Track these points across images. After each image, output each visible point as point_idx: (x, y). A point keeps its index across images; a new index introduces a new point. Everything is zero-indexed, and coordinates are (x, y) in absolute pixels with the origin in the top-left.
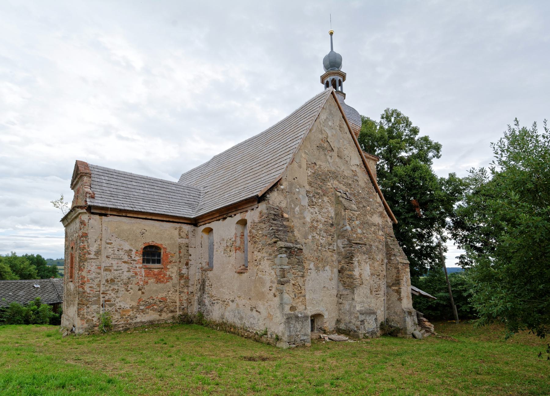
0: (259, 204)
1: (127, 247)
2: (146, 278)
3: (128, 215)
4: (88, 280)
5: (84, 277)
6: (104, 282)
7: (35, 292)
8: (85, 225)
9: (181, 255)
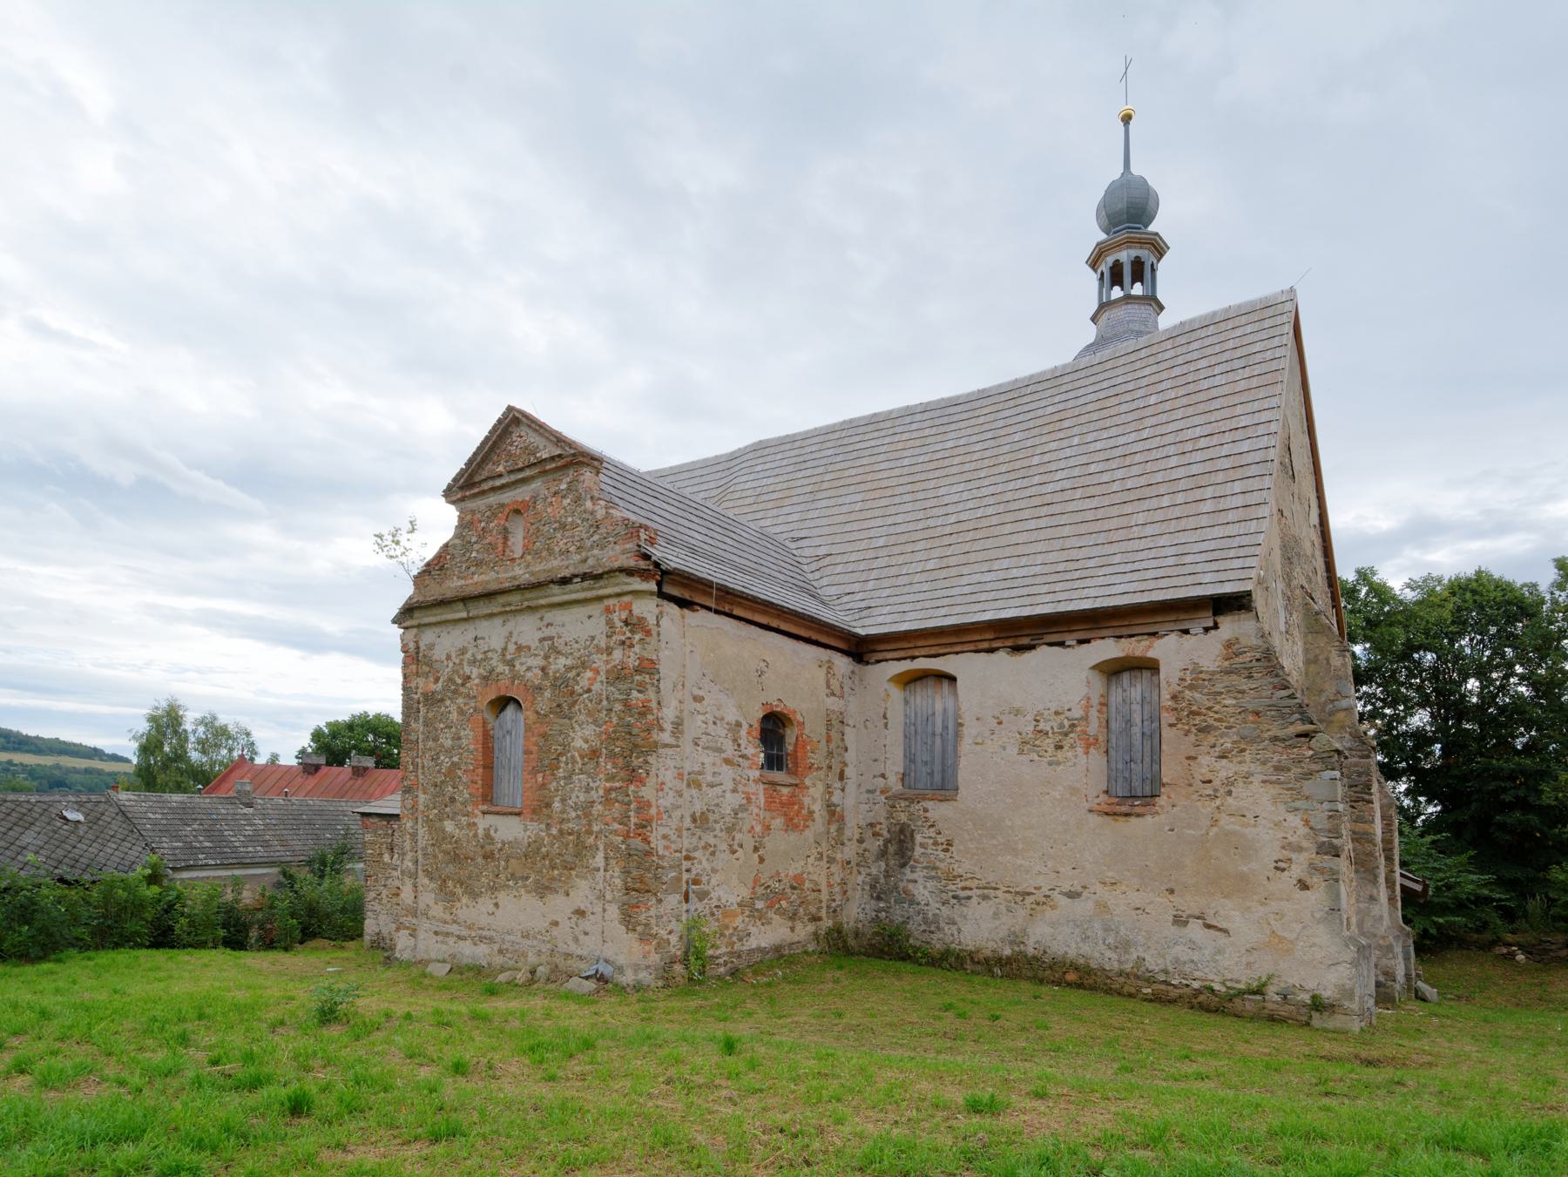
0: (1220, 619)
1: (732, 715)
2: (768, 814)
3: (737, 612)
4: (659, 813)
5: (649, 804)
6: (688, 822)
7: (73, 837)
8: (648, 633)
9: (832, 746)
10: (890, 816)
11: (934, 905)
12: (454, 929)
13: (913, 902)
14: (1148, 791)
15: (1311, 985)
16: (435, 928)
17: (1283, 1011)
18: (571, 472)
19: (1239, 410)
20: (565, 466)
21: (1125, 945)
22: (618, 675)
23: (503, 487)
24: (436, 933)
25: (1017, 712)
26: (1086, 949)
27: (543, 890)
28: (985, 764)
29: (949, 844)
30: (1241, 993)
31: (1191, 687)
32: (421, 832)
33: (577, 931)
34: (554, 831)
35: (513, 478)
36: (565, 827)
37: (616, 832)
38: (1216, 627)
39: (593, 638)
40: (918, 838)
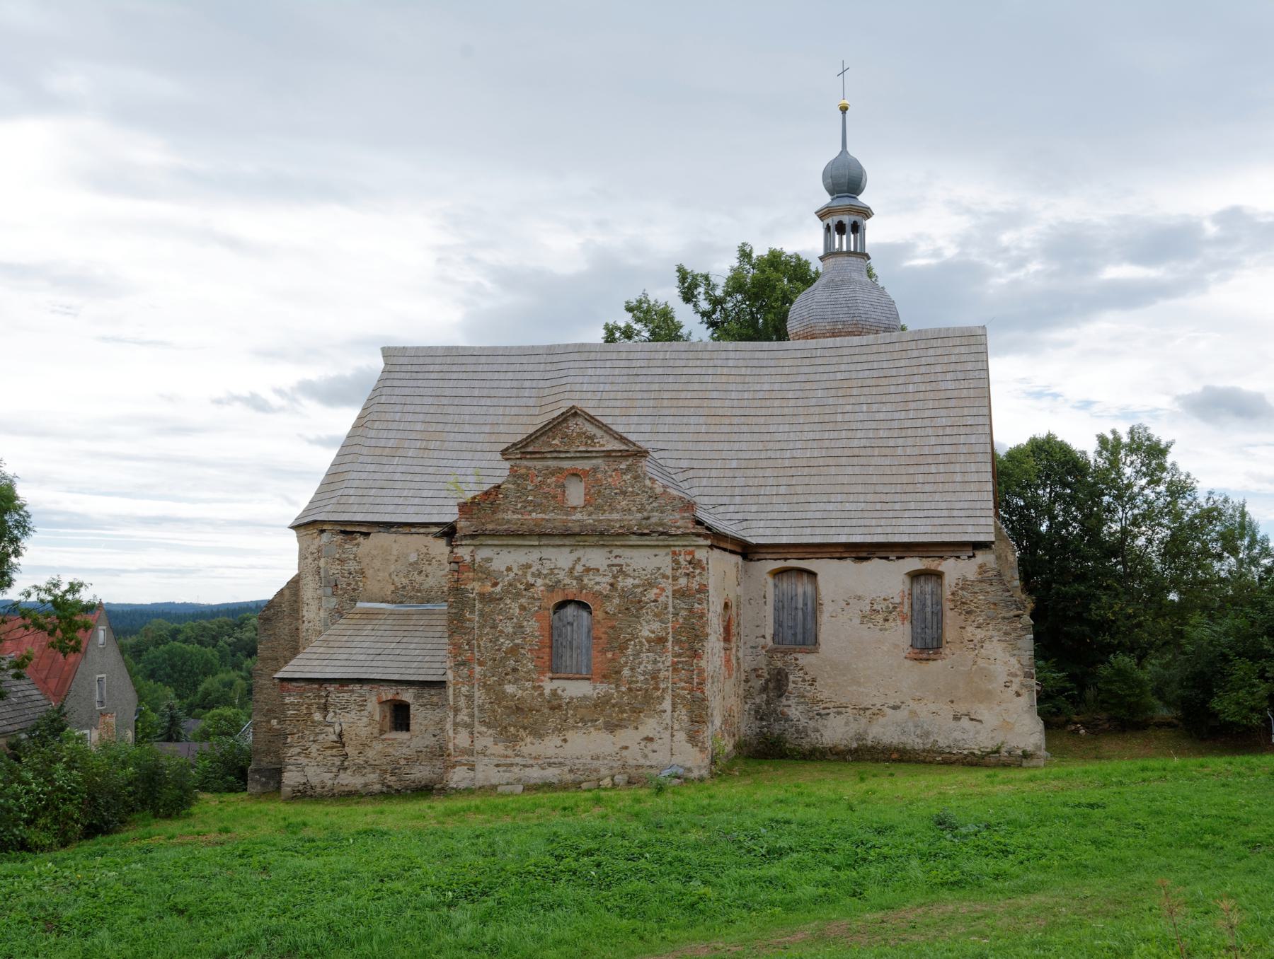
3: (722, 545)
8: (703, 569)
10: (769, 664)
11: (803, 720)
13: (787, 719)
14: (935, 644)
15: (1021, 745)
19: (966, 411)
21: (927, 734)
22: (680, 594)
24: (497, 766)
25: (859, 598)
26: (904, 739)
27: (611, 727)
28: (835, 628)
29: (814, 680)
30: (988, 753)
31: (962, 589)
32: (477, 694)
33: (646, 751)
34: (623, 689)
36: (634, 686)
37: (683, 688)
38: (974, 556)
40: (791, 678)
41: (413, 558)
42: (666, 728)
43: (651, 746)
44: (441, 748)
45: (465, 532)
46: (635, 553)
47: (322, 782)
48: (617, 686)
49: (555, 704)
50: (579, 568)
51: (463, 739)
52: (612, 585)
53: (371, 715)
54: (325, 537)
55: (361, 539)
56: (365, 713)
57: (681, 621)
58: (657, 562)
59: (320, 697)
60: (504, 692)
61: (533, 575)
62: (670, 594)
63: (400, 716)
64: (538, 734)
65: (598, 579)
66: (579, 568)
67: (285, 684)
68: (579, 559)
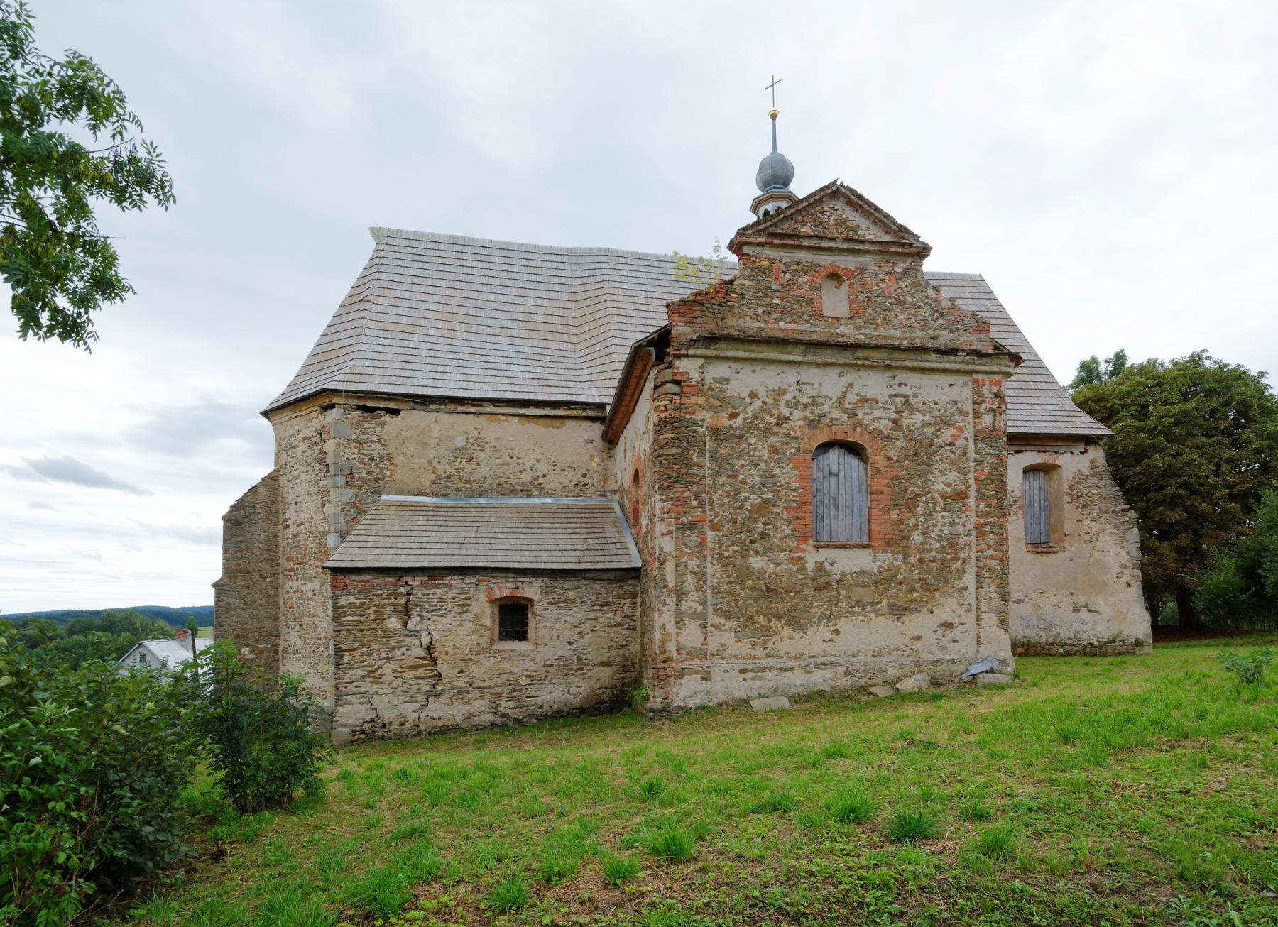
12: (771, 662)
15: (1134, 634)
16: (741, 667)
17: (1123, 649)
18: (909, 260)
20: (908, 255)
21: (1050, 627)
23: (830, 250)
24: (743, 671)
26: (1029, 633)
27: (899, 611)
31: (1078, 483)
32: (710, 571)
33: (945, 641)
34: (913, 560)
35: (846, 245)
37: (991, 557)
39: (956, 403)
41: (461, 441)
42: (969, 611)
43: (950, 634)
44: (579, 659)
45: (684, 339)
46: (925, 380)
47: (401, 716)
48: (905, 556)
49: (822, 583)
50: (851, 398)
51: (691, 635)
52: (895, 422)
53: (477, 618)
54: (334, 414)
55: (387, 417)
56: (469, 616)
57: (987, 470)
58: (953, 394)
59: (397, 595)
60: (748, 568)
61: (788, 404)
62: (971, 436)
63: (514, 619)
64: (796, 621)
65: (876, 413)
66: (851, 398)
67: (340, 577)
68: (851, 385)
